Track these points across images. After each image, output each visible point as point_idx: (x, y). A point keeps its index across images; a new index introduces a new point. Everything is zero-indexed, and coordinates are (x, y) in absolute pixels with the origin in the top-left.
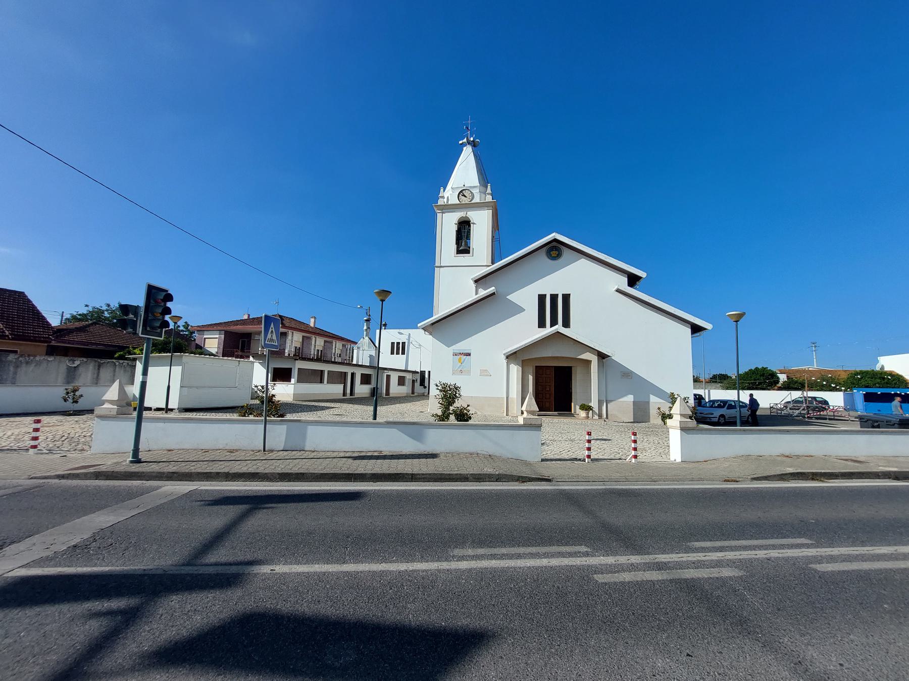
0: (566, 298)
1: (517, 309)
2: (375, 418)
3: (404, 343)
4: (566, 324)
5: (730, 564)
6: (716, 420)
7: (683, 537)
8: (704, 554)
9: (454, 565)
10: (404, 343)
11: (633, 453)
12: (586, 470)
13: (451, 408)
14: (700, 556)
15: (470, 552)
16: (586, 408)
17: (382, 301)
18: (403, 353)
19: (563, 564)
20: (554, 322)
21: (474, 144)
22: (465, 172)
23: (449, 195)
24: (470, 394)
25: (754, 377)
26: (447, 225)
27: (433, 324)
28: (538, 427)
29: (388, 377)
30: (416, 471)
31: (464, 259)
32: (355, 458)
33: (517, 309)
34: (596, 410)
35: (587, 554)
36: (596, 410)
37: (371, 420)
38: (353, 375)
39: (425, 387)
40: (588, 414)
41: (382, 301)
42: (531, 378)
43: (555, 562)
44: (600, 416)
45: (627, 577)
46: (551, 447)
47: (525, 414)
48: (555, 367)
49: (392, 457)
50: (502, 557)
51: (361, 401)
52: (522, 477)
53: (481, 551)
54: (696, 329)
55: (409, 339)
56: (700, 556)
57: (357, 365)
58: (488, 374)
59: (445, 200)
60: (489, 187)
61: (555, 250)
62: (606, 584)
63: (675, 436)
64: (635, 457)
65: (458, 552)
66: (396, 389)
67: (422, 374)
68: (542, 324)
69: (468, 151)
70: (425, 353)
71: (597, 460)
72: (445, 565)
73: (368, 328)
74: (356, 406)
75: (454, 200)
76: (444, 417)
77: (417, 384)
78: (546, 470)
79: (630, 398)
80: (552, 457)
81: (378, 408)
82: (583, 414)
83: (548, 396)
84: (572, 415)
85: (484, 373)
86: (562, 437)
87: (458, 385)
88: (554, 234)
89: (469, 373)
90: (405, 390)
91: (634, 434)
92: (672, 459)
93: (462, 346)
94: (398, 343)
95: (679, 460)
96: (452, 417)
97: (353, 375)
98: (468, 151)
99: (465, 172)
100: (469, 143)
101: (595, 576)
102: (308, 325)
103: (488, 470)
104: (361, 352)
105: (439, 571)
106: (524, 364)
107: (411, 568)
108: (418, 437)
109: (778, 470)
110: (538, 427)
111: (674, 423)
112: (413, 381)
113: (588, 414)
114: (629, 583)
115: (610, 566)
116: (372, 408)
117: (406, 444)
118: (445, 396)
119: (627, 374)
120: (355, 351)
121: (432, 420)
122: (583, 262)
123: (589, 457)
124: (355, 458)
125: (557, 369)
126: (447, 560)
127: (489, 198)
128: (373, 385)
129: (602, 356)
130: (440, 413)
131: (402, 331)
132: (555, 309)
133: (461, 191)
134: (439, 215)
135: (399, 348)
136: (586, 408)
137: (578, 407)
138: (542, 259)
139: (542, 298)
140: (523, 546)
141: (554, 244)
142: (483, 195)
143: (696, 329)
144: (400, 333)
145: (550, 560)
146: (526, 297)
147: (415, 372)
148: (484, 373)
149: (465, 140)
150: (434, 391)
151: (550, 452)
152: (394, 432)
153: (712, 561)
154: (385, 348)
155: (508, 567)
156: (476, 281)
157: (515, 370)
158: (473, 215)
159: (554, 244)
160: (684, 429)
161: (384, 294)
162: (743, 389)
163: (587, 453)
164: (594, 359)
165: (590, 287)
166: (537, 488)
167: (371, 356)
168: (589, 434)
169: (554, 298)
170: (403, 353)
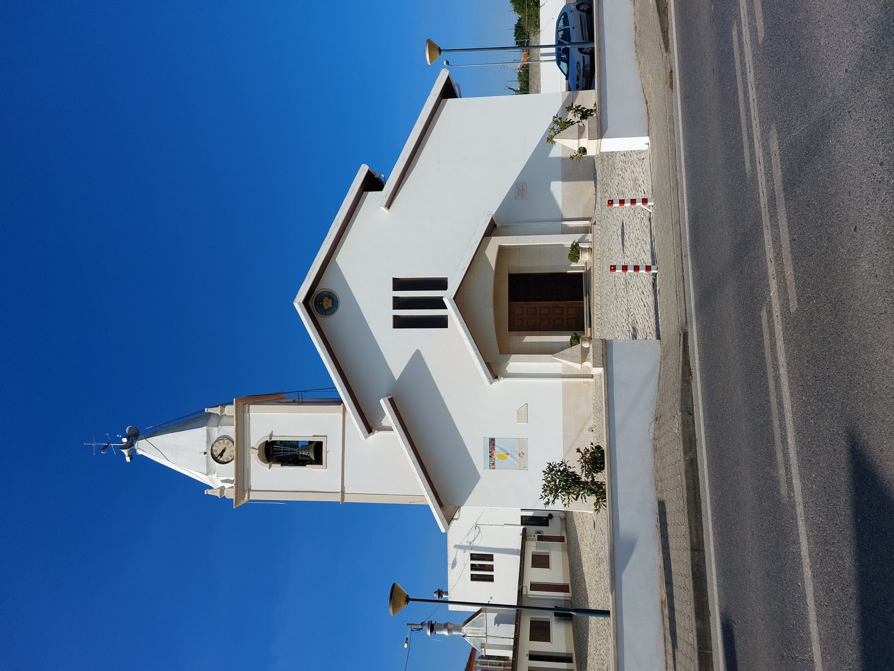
0: (399, 284)
1: (417, 361)
2: (606, 613)
3: (473, 557)
4: (441, 284)
5: (765, 140)
6: (587, 58)
7: (741, 185)
8: (758, 164)
9: (798, 498)
10: (473, 557)
11: (639, 204)
12: (666, 270)
13: (583, 479)
14: (760, 169)
15: (782, 472)
16: (575, 252)
17: (408, 599)
18: (490, 558)
19: (783, 348)
20: (439, 303)
21: (134, 437)
22: (180, 451)
23: (218, 480)
24: (557, 444)
26: (273, 482)
27: (441, 505)
28: (606, 345)
29: (535, 587)
30: (687, 544)
31: (331, 453)
32: (674, 645)
33: (417, 361)
34: (577, 237)
35: (770, 312)
37: (611, 620)
38: (533, 657)
39: (551, 516)
40: (584, 249)
41: (408, 599)
42: (529, 339)
43: (782, 359)
44: (587, 230)
45: (789, 271)
46: (639, 318)
47: (588, 364)
48: (509, 301)
49: (669, 583)
50: (783, 428)
51: (580, 640)
52: (683, 375)
53: (780, 456)
54: (449, 91)
55: (464, 548)
56: (760, 169)
57: (515, 648)
58: (527, 413)
59: (227, 485)
60: (210, 410)
61: (322, 303)
62: (799, 300)
63: (609, 145)
64: (645, 201)
65: (784, 491)
66: (556, 574)
67: (525, 521)
68: (441, 322)
69: (146, 448)
70: (491, 518)
71: (653, 255)
72: (800, 510)
73: (446, 626)
74: (591, 650)
75: (229, 470)
76: (598, 490)
77: (546, 531)
78: (670, 329)
79: (557, 188)
80: (653, 320)
81: (592, 606)
82: (585, 257)
83: (557, 311)
84: (588, 273)
85: (523, 414)
86: (623, 304)
87: (545, 467)
88: (296, 305)
89: (522, 442)
90: (557, 555)
91: (611, 203)
92: (646, 147)
93: (478, 453)
94: (473, 567)
95: (647, 139)
96: (600, 477)
97: (533, 657)
98: (146, 448)
99: (180, 451)
100: (130, 445)
101: (792, 310)
103: (676, 426)
104: (490, 641)
105: (807, 520)
106: (506, 350)
107: (808, 560)
108: (630, 546)
109: (653, 14)
110: (606, 345)
111: (592, 148)
112: (541, 538)
114: (795, 270)
115: (779, 287)
116: (593, 619)
117: (645, 564)
118: (564, 489)
119: (520, 189)
120: (490, 652)
121: (605, 512)
122: (341, 259)
123: (648, 268)
124: (674, 645)
125: (512, 298)
126: (794, 507)
127: (230, 410)
128: (550, 616)
129: (492, 230)
130: (593, 499)
131: (450, 561)
132: (417, 302)
133: (215, 459)
134: (254, 496)
135: (482, 567)
136: (575, 252)
137: (574, 265)
138: (336, 321)
139: (400, 323)
140: (768, 395)
141: (311, 303)
142: (224, 420)
143: (449, 91)
144: (454, 564)
145: (780, 364)
146: (396, 348)
147: (525, 536)
148: (523, 414)
149: (125, 452)
150: (558, 505)
151: (646, 324)
152: (626, 577)
153: (763, 154)
154: (482, 592)
155: (794, 422)
156: (370, 430)
157: (515, 364)
158: (257, 437)
159: (311, 303)
160: (600, 133)
161: (396, 597)
163: (642, 271)
164: (496, 242)
166: (697, 356)
167: (498, 621)
168: (613, 268)
169: (398, 303)
170: (490, 558)
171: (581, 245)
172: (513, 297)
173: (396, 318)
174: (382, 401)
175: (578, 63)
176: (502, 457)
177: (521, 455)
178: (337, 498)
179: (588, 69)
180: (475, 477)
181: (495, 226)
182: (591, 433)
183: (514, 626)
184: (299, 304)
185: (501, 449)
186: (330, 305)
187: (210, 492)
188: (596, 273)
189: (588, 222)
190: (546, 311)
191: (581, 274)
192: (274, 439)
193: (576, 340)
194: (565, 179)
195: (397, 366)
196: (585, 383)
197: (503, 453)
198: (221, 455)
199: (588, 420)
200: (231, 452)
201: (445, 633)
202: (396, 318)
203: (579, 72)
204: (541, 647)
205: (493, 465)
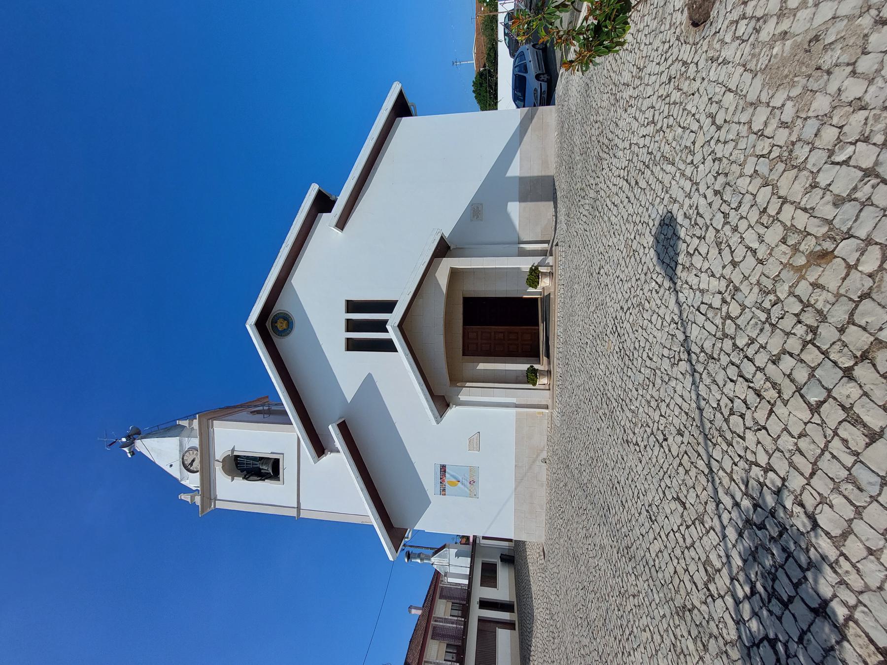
1: (369, 385)
4: (388, 306)
16: (534, 276)
22: (163, 451)
25: (483, 93)
26: (235, 493)
31: (288, 469)
33: (369, 385)
34: (536, 260)
36: (536, 260)
40: (544, 274)
42: (482, 366)
44: (544, 253)
54: (402, 109)
57: (470, 577)
60: (182, 423)
61: (275, 324)
68: (387, 346)
73: (419, 556)
79: (514, 209)
82: (545, 282)
84: (547, 299)
85: (475, 443)
88: (248, 327)
89: (473, 470)
90: (504, 575)
93: (429, 480)
98: (144, 446)
99: (163, 451)
100: (130, 443)
102: (422, 615)
104: (453, 570)
106: (457, 379)
113: (544, 274)
119: (475, 211)
122: (297, 280)
125: (467, 321)
129: (443, 249)
132: (366, 325)
134: (219, 505)
136: (534, 276)
137: (531, 290)
139: (353, 345)
143: (402, 109)
146: (349, 372)
148: (475, 443)
158: (221, 450)
162: (497, 10)
164: (446, 264)
165: (337, 270)
167: (458, 555)
169: (352, 326)
171: (542, 269)
172: (468, 320)
173: (348, 340)
174: (330, 427)
175: (536, 90)
176: (452, 484)
177: (472, 482)
178: (293, 513)
179: (545, 96)
180: (426, 502)
181: (449, 247)
182: (544, 464)
183: (469, 559)
184: (251, 326)
185: (452, 476)
186: (285, 327)
187: (186, 497)
188: (558, 301)
189: (546, 245)
190: (501, 335)
191: (536, 299)
192: (236, 453)
193: (531, 376)
194: (523, 199)
195: (349, 389)
196: (539, 413)
197: (454, 480)
198: (191, 464)
199: (542, 450)
200: (196, 465)
201: (419, 561)
202: (348, 340)
203: (536, 98)
204: (489, 593)
205: (443, 491)
